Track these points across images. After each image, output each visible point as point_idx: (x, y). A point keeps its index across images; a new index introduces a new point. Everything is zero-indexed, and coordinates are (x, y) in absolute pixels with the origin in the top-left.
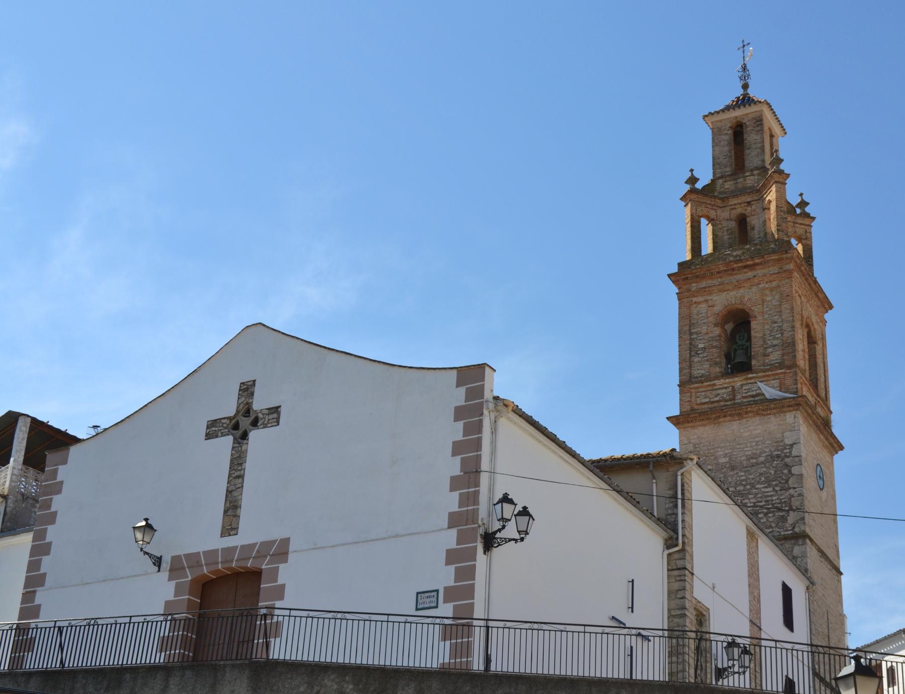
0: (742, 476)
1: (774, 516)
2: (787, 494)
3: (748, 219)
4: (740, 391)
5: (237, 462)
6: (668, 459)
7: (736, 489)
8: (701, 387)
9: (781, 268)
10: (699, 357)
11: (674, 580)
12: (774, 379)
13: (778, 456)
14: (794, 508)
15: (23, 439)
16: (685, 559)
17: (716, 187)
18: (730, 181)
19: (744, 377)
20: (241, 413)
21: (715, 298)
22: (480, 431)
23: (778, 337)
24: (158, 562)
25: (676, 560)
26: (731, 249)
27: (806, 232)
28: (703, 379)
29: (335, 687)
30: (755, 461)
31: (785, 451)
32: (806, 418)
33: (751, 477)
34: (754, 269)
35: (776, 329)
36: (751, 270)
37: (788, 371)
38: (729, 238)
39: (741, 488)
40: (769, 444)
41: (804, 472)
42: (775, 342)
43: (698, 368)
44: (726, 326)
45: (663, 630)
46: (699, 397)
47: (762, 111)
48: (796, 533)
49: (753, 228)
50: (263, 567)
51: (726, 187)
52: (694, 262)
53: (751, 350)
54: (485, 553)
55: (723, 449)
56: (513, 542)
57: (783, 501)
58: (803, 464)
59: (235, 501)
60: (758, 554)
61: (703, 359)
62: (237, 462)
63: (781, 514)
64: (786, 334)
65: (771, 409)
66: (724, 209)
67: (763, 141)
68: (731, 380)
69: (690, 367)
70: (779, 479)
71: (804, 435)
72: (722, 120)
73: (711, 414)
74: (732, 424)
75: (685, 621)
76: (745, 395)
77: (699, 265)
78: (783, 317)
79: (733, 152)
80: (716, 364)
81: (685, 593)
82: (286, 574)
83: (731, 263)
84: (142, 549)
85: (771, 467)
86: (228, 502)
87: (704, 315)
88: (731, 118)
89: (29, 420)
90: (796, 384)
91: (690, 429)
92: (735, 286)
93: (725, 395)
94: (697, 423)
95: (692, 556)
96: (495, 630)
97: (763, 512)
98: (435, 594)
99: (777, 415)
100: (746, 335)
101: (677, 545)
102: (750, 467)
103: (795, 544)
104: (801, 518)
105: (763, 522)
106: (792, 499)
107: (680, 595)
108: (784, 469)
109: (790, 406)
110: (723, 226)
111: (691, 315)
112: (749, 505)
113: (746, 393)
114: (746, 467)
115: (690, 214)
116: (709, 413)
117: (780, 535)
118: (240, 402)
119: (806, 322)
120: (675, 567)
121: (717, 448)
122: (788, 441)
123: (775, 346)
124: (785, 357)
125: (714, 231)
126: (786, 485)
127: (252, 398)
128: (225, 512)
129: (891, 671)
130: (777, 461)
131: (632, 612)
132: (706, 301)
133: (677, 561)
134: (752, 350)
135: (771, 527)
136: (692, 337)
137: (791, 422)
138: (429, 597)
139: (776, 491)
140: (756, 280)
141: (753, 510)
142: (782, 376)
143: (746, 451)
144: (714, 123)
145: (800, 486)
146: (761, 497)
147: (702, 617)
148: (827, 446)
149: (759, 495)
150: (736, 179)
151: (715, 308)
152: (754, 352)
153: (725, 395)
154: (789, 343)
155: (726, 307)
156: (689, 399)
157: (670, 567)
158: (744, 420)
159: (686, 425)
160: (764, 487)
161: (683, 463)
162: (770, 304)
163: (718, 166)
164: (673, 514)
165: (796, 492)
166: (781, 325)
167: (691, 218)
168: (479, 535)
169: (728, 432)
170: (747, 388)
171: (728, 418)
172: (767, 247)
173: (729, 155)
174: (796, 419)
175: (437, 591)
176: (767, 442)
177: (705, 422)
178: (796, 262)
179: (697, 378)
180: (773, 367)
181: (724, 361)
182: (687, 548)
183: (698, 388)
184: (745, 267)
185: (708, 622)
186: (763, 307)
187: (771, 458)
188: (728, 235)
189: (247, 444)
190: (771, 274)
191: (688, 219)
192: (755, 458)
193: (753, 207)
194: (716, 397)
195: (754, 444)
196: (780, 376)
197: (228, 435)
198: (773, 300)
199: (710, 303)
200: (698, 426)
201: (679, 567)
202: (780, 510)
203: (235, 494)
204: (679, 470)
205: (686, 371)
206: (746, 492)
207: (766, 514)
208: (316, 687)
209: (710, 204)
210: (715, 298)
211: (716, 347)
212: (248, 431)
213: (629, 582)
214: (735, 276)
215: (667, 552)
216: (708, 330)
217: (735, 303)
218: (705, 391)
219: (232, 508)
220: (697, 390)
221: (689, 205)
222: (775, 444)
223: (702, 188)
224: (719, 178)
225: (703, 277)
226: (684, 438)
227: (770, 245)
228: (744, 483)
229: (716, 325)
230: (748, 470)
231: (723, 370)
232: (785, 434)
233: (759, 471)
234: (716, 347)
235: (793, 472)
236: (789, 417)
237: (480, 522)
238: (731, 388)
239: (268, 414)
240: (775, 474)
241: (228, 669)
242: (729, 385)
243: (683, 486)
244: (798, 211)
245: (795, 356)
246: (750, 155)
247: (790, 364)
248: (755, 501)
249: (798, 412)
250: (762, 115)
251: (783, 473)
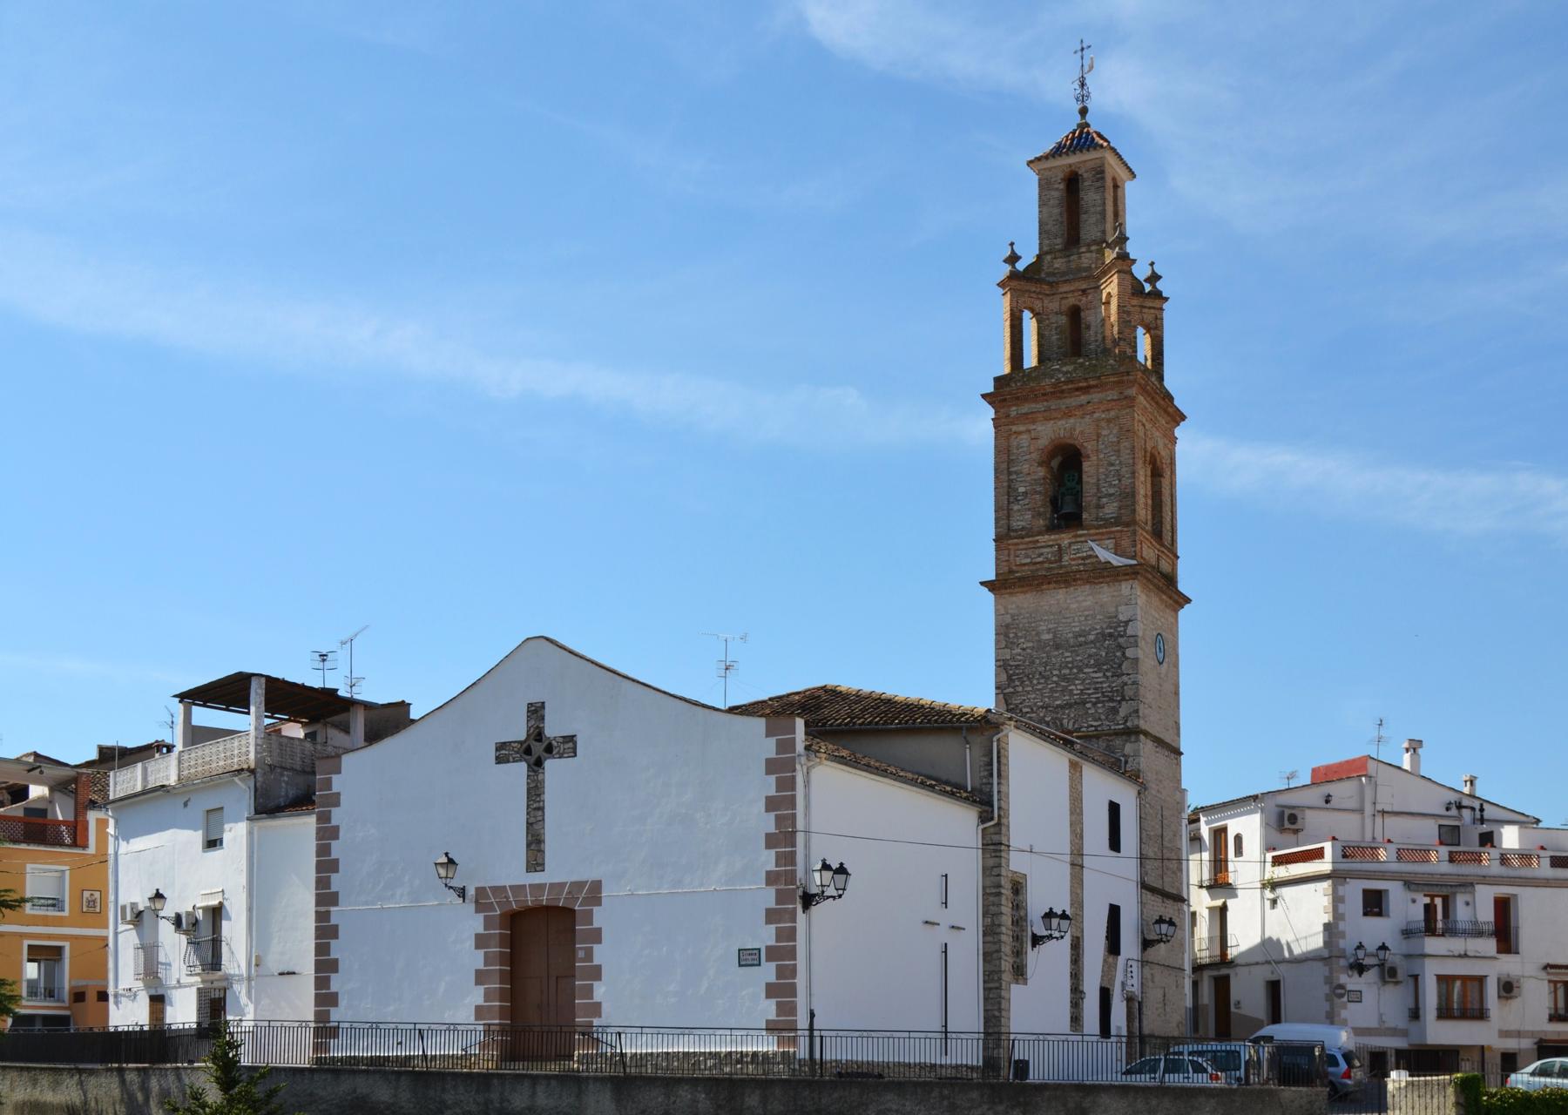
0: (1068, 657)
1: (1104, 706)
3: (1082, 314)
5: (535, 792)
8: (1022, 543)
9: (1121, 393)
13: (1111, 635)
15: (260, 704)
16: (1000, 834)
18: (1061, 257)
20: (532, 737)
21: (1039, 428)
22: (793, 788)
24: (462, 893)
25: (991, 834)
27: (1156, 318)
28: (1023, 533)
29: (689, 1096)
30: (1082, 639)
31: (1119, 629)
33: (1078, 658)
34: (1088, 393)
35: (1112, 473)
36: (1084, 394)
37: (1125, 529)
38: (1058, 339)
39: (1067, 671)
41: (1140, 654)
42: (1112, 491)
46: (1018, 556)
48: (1128, 728)
49: (1088, 327)
50: (576, 908)
51: (1056, 266)
52: (1014, 378)
54: (804, 912)
56: (831, 899)
58: (1139, 645)
59: (538, 835)
60: (1082, 784)
62: (535, 792)
63: (1111, 705)
64: (1126, 481)
65: (1104, 577)
67: (1105, 203)
68: (1057, 536)
69: (1008, 517)
76: (1074, 556)
77: (1019, 381)
79: (1065, 216)
80: (1039, 514)
82: (600, 918)
84: (446, 885)
86: (530, 835)
87: (1025, 449)
88: (1064, 165)
89: (263, 680)
90: (1135, 546)
92: (1065, 413)
93: (1050, 556)
94: (1016, 590)
99: (1111, 584)
100: (1076, 474)
101: (992, 819)
102: (1078, 646)
103: (1126, 741)
106: (1125, 687)
107: (995, 871)
108: (1117, 651)
109: (1127, 574)
112: (1075, 692)
114: (1073, 647)
115: (1008, 308)
117: (1110, 729)
118: (530, 725)
123: (1111, 495)
124: (1123, 511)
125: (1039, 328)
127: (543, 723)
128: (528, 845)
129: (1238, 839)
131: (946, 907)
132: (1029, 431)
133: (993, 836)
134: (1084, 499)
135: (1100, 719)
136: (1012, 477)
137: (1127, 594)
138: (752, 954)
139: (1107, 678)
142: (1118, 535)
144: (1042, 172)
145: (1135, 672)
146: (1089, 684)
147: (1018, 887)
149: (1087, 681)
150: (1069, 256)
151: (1039, 441)
153: (1050, 556)
156: (1007, 558)
157: (985, 842)
158: (1072, 588)
159: (1003, 591)
164: (989, 784)
165: (1130, 679)
167: (1011, 314)
168: (798, 898)
169: (1052, 602)
175: (759, 950)
176: (1098, 617)
178: (1140, 384)
179: (1016, 531)
180: (1107, 523)
182: (1004, 821)
184: (1077, 389)
189: (544, 773)
191: (1007, 315)
192: (1084, 636)
193: (1090, 297)
195: (1083, 618)
197: (521, 761)
198: (1109, 434)
199: (1033, 435)
200: (1017, 592)
202: (1111, 700)
203: (535, 827)
204: (994, 736)
207: (1094, 704)
208: (672, 1097)
210: (1039, 428)
211: (1040, 493)
212: (542, 758)
214: (1064, 400)
215: (981, 827)
217: (1064, 437)
218: (1026, 549)
219: (535, 842)
220: (1017, 547)
221: (1009, 295)
222: (1106, 620)
224: (1047, 253)
225: (1025, 399)
228: (1070, 665)
229: (1040, 464)
230: (1075, 651)
231: (1047, 522)
234: (1040, 493)
235: (1127, 655)
237: (798, 884)
239: (563, 743)
241: (591, 1082)
242: (1054, 543)
243: (999, 752)
244: (1148, 288)
246: (1087, 223)
250: (1103, 164)
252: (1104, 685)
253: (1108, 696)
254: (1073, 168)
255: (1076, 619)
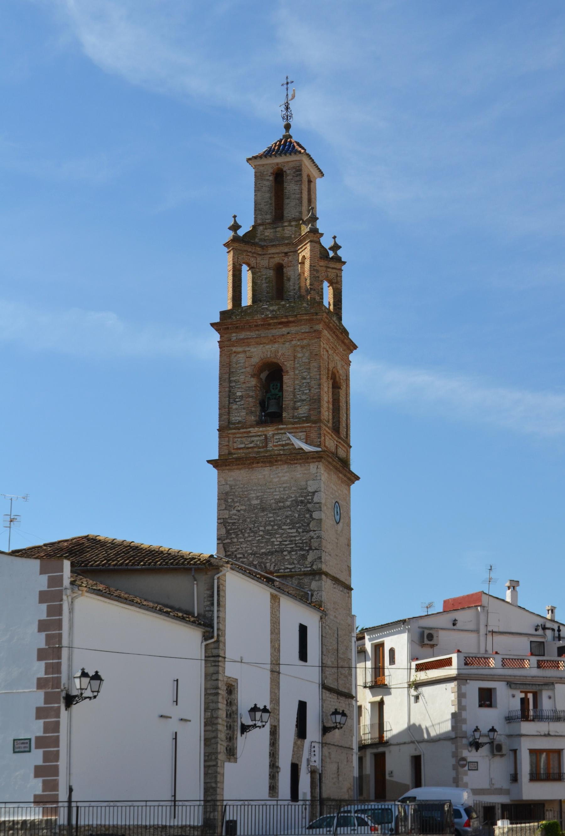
0: (271, 517)
2: (308, 535)
3: (285, 270)
4: (272, 440)
6: (207, 566)
7: (265, 528)
8: (238, 433)
9: (311, 328)
10: (236, 404)
11: (210, 665)
12: (301, 432)
13: (302, 502)
14: (313, 548)
17: (257, 234)
18: (270, 228)
19: (275, 427)
22: (60, 614)
23: (306, 393)
25: (212, 649)
26: (268, 303)
27: (337, 276)
28: (240, 425)
30: (282, 504)
31: (308, 498)
32: (327, 466)
36: (285, 326)
37: (313, 425)
38: (267, 287)
39: (270, 528)
40: (295, 490)
41: (323, 516)
42: (304, 397)
43: (236, 414)
44: (262, 374)
45: (200, 801)
46: (235, 442)
47: (301, 161)
48: (314, 570)
49: (289, 280)
51: (266, 234)
52: (235, 313)
53: (282, 402)
54: (66, 710)
55: (255, 492)
56: (88, 699)
57: (304, 541)
61: (240, 407)
63: (302, 553)
65: (297, 459)
66: (263, 256)
68: (264, 429)
69: (229, 413)
70: (302, 522)
71: (324, 483)
72: (264, 164)
73: (246, 460)
74: (264, 470)
75: (218, 699)
76: (276, 444)
77: (239, 315)
78: (311, 375)
79: (273, 199)
80: (252, 412)
81: (218, 676)
83: (268, 319)
85: (296, 512)
87: (242, 364)
88: (273, 163)
90: (320, 438)
91: (227, 471)
92: (271, 340)
93: (258, 443)
95: (225, 643)
96: (83, 808)
97: (287, 550)
98: (28, 741)
99: (302, 464)
100: (279, 385)
101: (212, 637)
102: (278, 510)
103: (312, 579)
104: (318, 557)
105: (287, 559)
108: (307, 514)
110: (262, 273)
111: (231, 364)
112: (276, 543)
113: (277, 442)
114: (275, 510)
115: (231, 263)
116: (244, 459)
117: (300, 571)
119: (332, 371)
120: (210, 655)
121: (250, 490)
122: (310, 489)
123: (303, 400)
124: (312, 412)
125: (253, 278)
126: (308, 528)
130: (301, 506)
131: (177, 704)
132: (245, 352)
134: (284, 402)
135: (293, 563)
136: (232, 385)
139: (299, 533)
140: (289, 337)
141: (279, 548)
143: (275, 495)
144: (257, 167)
145: (319, 529)
146: (286, 537)
148: (345, 480)
149: (285, 535)
150: (276, 228)
151: (252, 360)
152: (285, 405)
153: (258, 443)
154: (315, 399)
155: (262, 359)
156: (227, 444)
157: (207, 655)
159: (224, 468)
160: (289, 529)
161: (219, 569)
162: (300, 360)
163: (259, 212)
164: (210, 611)
165: (315, 534)
166: (309, 381)
169: (260, 477)
170: (277, 437)
171: (260, 465)
172: (300, 306)
173: (270, 202)
174: (318, 470)
175: (30, 740)
176: (293, 488)
177: (240, 467)
178: (325, 322)
179: (234, 424)
180: (301, 420)
181: (259, 409)
182: (221, 639)
183: (235, 434)
184: (281, 323)
185: (236, 690)
186: (294, 362)
187: (296, 503)
188: (267, 283)
190: (302, 333)
191: (230, 267)
192: (283, 502)
193: (290, 258)
194: (251, 443)
195: (282, 489)
196: (306, 428)
198: (303, 357)
199: (248, 354)
200: (234, 469)
201: (214, 655)
202: (302, 549)
204: (215, 575)
205: (225, 417)
206: (274, 532)
207: (290, 552)
209: (250, 252)
211: (252, 397)
213: (174, 681)
215: (204, 643)
216: (245, 379)
220: (234, 436)
222: (300, 491)
223: (243, 235)
224: (260, 225)
225: (243, 329)
226: (221, 479)
227: (303, 304)
228: (272, 523)
229: (252, 376)
230: (276, 512)
232: (309, 482)
233: (285, 514)
234: (252, 397)
235: (314, 516)
236: (313, 468)
237: (62, 687)
238: (264, 436)
240: (298, 517)
242: (262, 434)
243: (218, 587)
244: (331, 254)
245: (320, 412)
247: (315, 419)
248: (281, 540)
249: (321, 463)
251: (305, 517)
252: (297, 538)
253: (299, 546)
254: (280, 166)
255: (277, 490)
